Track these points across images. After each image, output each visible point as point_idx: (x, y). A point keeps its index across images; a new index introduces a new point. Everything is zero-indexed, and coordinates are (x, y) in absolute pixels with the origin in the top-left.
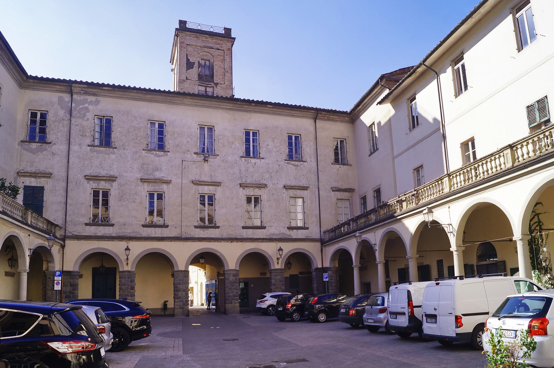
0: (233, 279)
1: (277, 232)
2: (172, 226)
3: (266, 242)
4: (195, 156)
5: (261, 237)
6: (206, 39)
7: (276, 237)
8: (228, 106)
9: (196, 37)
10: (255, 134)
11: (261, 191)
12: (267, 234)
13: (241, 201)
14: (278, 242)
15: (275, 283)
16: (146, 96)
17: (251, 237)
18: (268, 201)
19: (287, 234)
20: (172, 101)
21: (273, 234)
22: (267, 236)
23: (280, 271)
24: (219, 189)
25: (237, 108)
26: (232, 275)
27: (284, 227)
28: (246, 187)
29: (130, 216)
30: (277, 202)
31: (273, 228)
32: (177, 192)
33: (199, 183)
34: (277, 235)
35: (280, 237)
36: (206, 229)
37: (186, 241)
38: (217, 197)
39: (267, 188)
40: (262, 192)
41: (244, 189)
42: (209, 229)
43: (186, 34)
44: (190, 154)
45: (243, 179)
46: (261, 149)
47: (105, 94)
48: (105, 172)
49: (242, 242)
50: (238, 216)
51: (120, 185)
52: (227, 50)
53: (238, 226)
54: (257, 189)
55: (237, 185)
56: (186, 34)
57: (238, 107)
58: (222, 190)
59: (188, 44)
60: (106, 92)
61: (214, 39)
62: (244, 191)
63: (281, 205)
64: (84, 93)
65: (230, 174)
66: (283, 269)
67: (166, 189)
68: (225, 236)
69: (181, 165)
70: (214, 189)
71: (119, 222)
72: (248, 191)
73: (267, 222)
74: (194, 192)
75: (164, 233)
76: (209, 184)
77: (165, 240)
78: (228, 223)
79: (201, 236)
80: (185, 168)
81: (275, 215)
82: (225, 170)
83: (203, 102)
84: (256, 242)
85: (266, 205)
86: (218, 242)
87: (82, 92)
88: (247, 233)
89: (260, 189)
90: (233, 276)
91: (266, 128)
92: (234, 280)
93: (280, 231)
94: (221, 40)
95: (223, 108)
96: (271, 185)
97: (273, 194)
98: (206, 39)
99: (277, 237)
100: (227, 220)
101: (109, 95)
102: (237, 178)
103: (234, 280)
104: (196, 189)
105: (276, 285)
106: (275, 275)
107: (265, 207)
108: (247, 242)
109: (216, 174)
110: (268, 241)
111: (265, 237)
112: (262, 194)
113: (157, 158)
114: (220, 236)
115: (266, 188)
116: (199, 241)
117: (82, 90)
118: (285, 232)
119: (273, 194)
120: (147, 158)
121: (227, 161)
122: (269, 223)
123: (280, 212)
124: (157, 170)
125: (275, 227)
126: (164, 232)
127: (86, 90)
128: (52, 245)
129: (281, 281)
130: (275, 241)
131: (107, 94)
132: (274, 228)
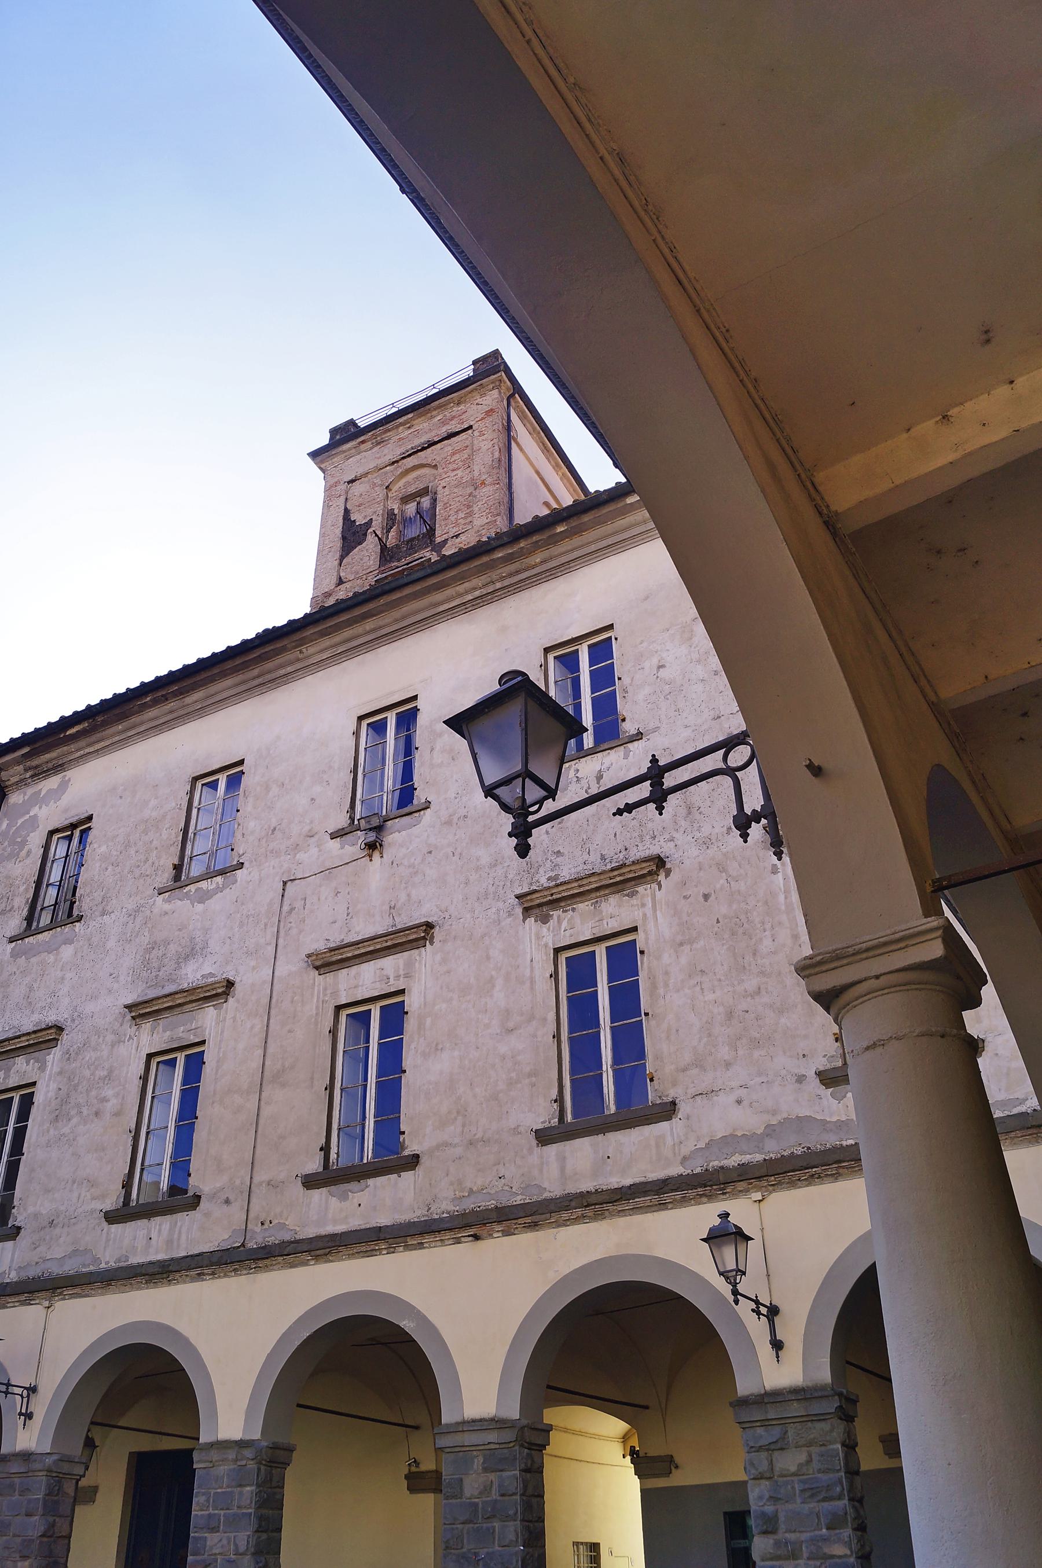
0: (486, 1489)
1: (751, 1121)
2: (213, 1196)
3: (684, 1202)
4: (336, 844)
5: (653, 1176)
6: (412, 430)
7: (746, 1159)
8: (467, 592)
9: (378, 443)
10: (602, 651)
11: (634, 901)
12: (686, 1150)
13: (532, 988)
14: (759, 1189)
15: (769, 1509)
16: (188, 700)
17: (587, 1185)
18: (681, 944)
19: (824, 1122)
20: (269, 677)
21: (730, 1141)
22: (685, 1159)
23: (796, 1409)
24: (426, 957)
25: (506, 582)
26: (478, 1462)
27: (801, 1079)
28: (554, 903)
29: (74, 1182)
30: (733, 934)
31: (722, 1099)
32: (252, 1028)
33: (334, 959)
34: (753, 1139)
35: (773, 1149)
36: (353, 1185)
37: (260, 1264)
38: (412, 1002)
39: (667, 875)
40: (643, 905)
41: (545, 919)
42: (371, 1182)
43: (344, 452)
44: (318, 846)
45: (541, 871)
46: (629, 695)
47: (82, 752)
48: (36, 1017)
49: (534, 1226)
50: (513, 1075)
51: (68, 1056)
52: (482, 419)
53: (516, 1131)
54: (613, 900)
55: (510, 914)
56: (344, 452)
57: (511, 575)
58: (438, 957)
59: (352, 477)
60: (82, 743)
61: (434, 413)
62: (545, 930)
63: (767, 945)
64: (32, 776)
65: (478, 869)
66: (823, 1388)
67: (213, 1024)
68: (444, 1206)
69: (277, 906)
70: (401, 967)
71: (36, 1216)
72: (564, 924)
73: (684, 1070)
74: (317, 1008)
75: (179, 1239)
76: (378, 947)
77: (178, 1275)
78: (464, 1126)
79: (331, 1229)
80: (292, 909)
81: (730, 1015)
82: (456, 858)
83: (369, 624)
84: (621, 1213)
85: (667, 973)
86: (408, 1248)
87: (28, 775)
88: (563, 1169)
89: (631, 895)
90: (486, 1470)
91: (646, 598)
92: (495, 1495)
93: (774, 1112)
94: (459, 404)
95: (450, 613)
96: (694, 852)
97: (706, 897)
98: (412, 430)
99: (759, 1157)
100: (458, 1112)
101: (91, 749)
102: (510, 876)
103: (495, 1495)
104: (325, 989)
105: (782, 1527)
106: (763, 1442)
107: (666, 985)
108: (565, 1223)
109: (414, 892)
110: (691, 1193)
111: (676, 1170)
112: (645, 915)
113: (199, 907)
114: (418, 1213)
115: (661, 877)
116: (317, 1258)
117: (26, 770)
118: (803, 1112)
119: (706, 897)
120: (167, 917)
121: (465, 817)
122: (695, 1071)
123: (758, 991)
124: (190, 953)
125: (742, 1093)
126: (180, 1232)
127: (35, 762)
128: (82, 1474)
129: (812, 1492)
130: (742, 1185)
131: (87, 750)
132: (733, 1098)
